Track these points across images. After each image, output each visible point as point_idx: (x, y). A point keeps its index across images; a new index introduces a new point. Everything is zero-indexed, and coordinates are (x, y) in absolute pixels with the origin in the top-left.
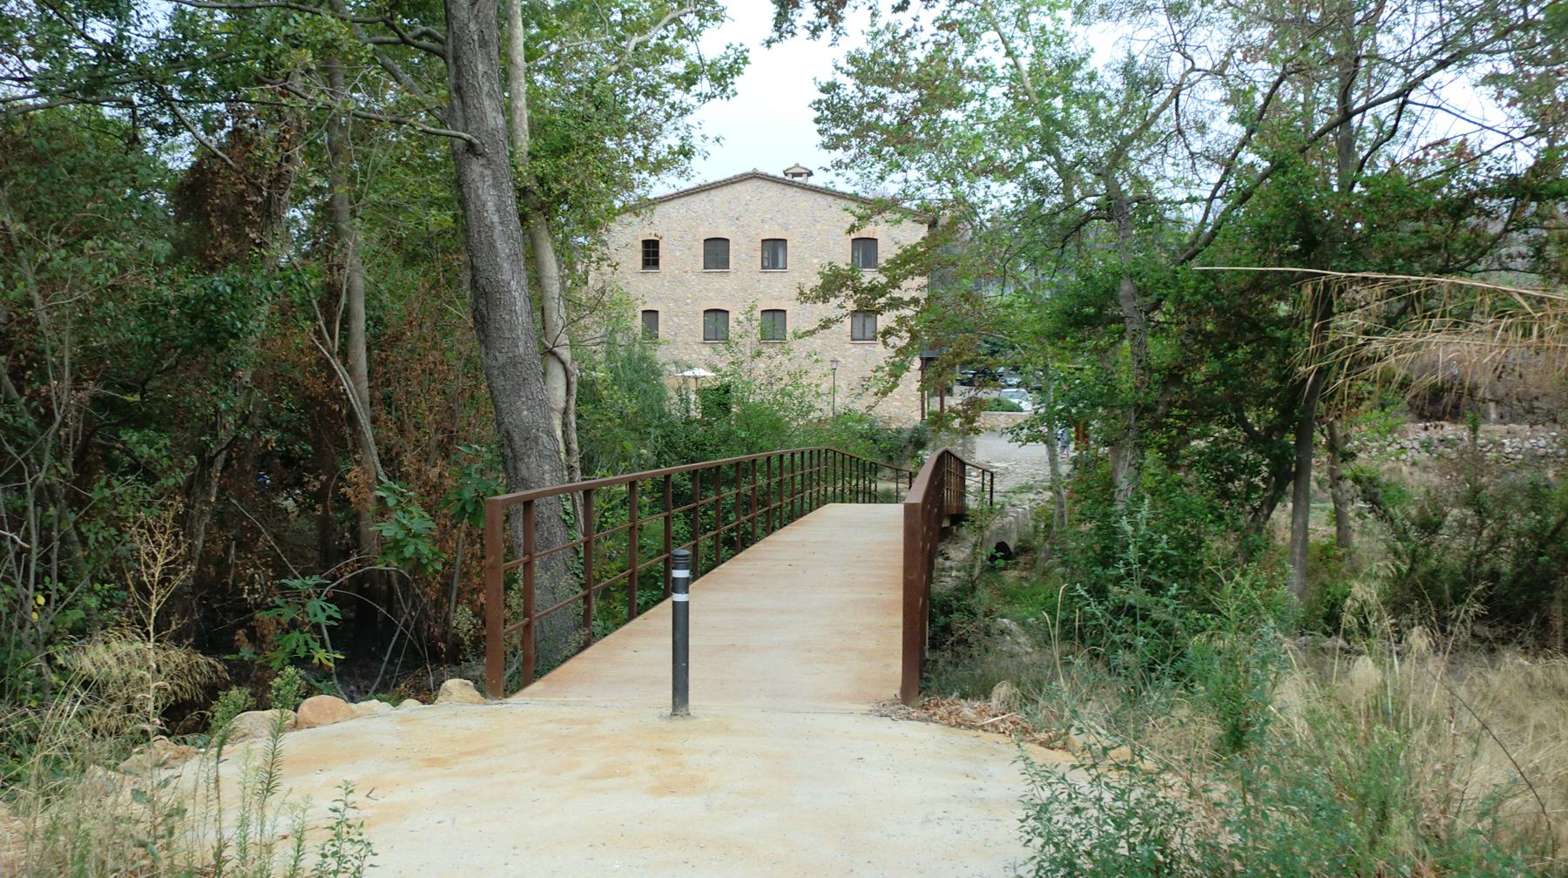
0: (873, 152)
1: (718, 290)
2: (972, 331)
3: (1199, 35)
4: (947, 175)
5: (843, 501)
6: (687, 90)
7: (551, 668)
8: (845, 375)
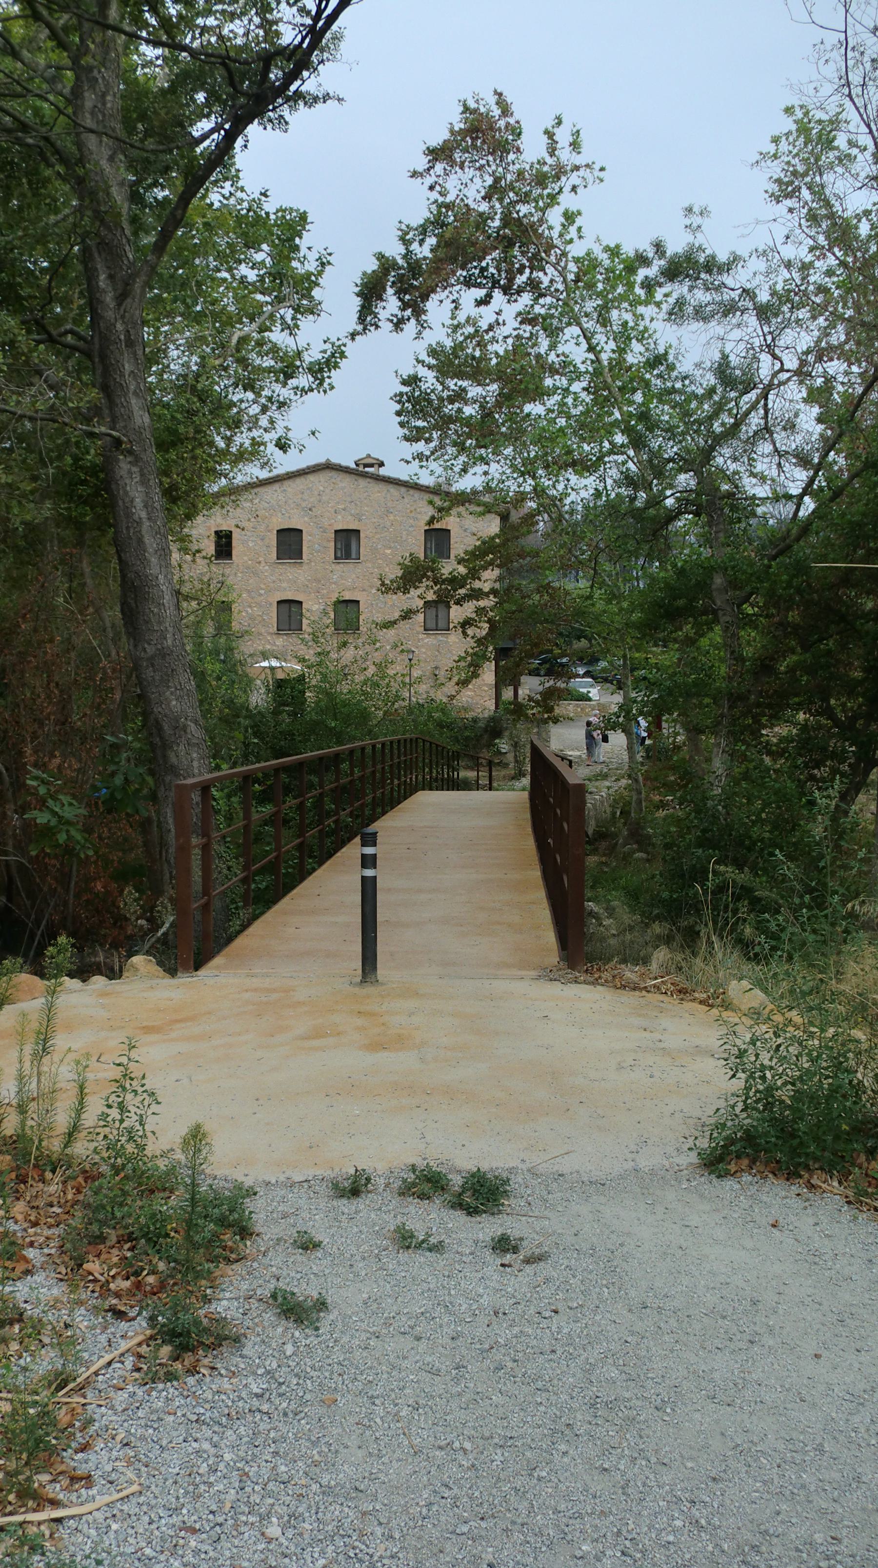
0: (455, 444)
1: (290, 581)
2: (552, 622)
3: (788, 337)
4: (527, 470)
5: (431, 789)
6: (285, 384)
7: (230, 940)
8: (431, 664)
